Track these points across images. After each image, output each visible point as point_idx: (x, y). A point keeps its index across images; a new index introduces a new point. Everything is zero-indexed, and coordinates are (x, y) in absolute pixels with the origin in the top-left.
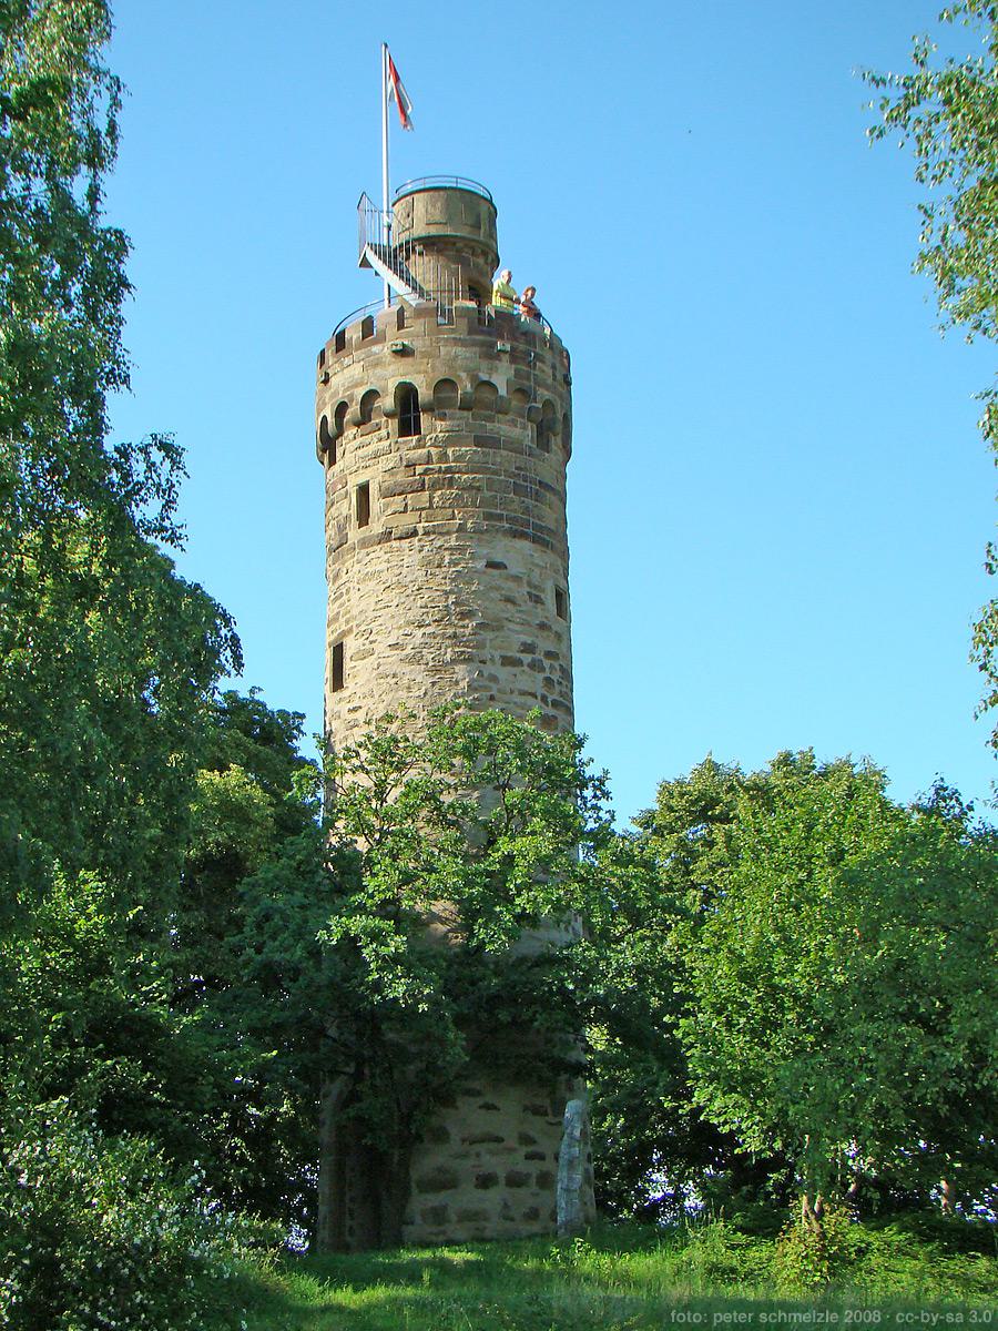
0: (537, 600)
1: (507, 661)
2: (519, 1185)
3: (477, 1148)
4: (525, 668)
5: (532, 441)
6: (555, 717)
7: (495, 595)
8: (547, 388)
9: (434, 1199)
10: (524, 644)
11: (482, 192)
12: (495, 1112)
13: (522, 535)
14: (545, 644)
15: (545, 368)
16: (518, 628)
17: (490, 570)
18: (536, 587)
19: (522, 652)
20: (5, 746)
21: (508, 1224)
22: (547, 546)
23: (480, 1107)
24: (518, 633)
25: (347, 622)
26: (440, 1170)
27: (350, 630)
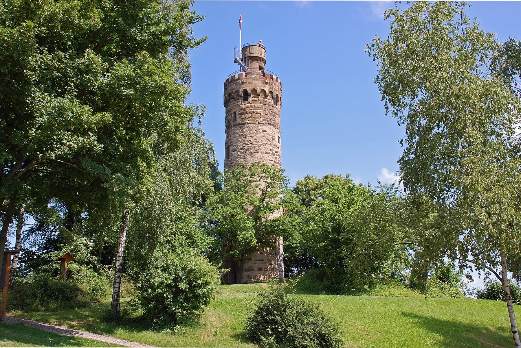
8: (277, 91)
27: (231, 145)
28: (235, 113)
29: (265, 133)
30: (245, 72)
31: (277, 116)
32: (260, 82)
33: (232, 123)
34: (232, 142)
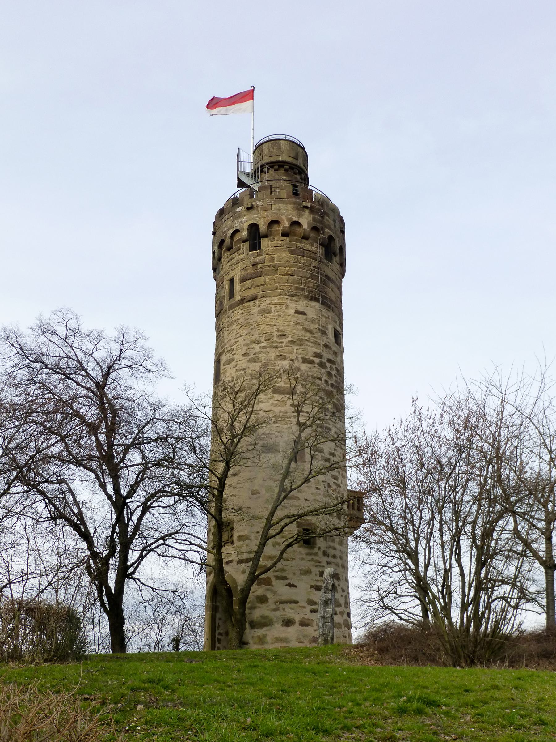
0: (324, 333)
1: (305, 361)
2: (307, 625)
3: (281, 606)
4: (316, 365)
5: (322, 255)
6: (332, 392)
7: (300, 327)
8: (330, 229)
9: (259, 632)
10: (315, 353)
11: (298, 142)
12: (294, 588)
13: (316, 300)
14: (327, 355)
15: (330, 220)
16: (311, 345)
17: (296, 315)
18: (322, 326)
19: (314, 357)
20: (411, 741)
21: (301, 645)
22: (330, 308)
23: (286, 585)
24: (312, 347)
25: (222, 348)
26: (262, 617)
27: (224, 351)
28: (232, 281)
29: (300, 316)
30: (233, 423)
31: (331, 285)
32: (290, 206)
33: (226, 304)
34: (226, 345)
